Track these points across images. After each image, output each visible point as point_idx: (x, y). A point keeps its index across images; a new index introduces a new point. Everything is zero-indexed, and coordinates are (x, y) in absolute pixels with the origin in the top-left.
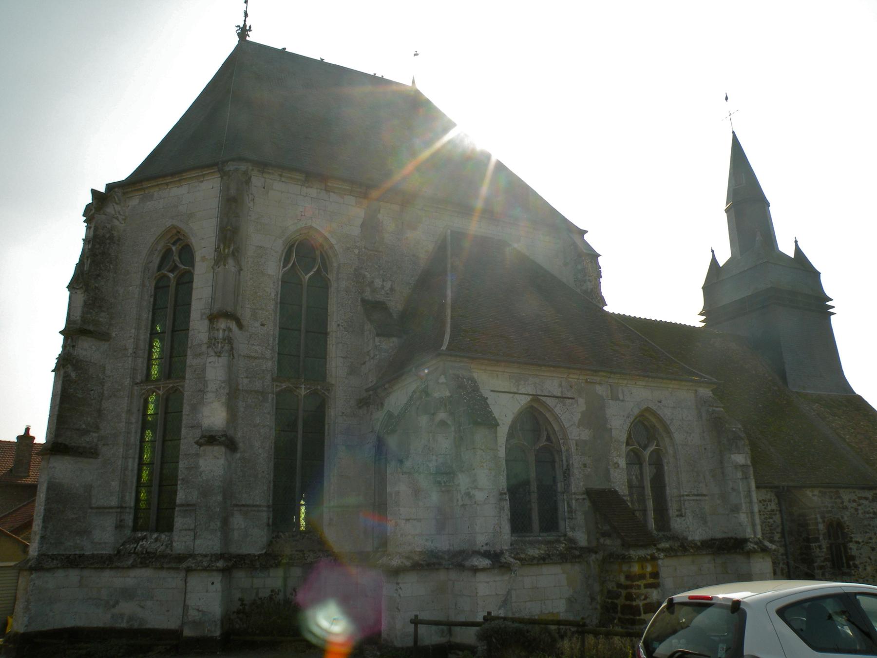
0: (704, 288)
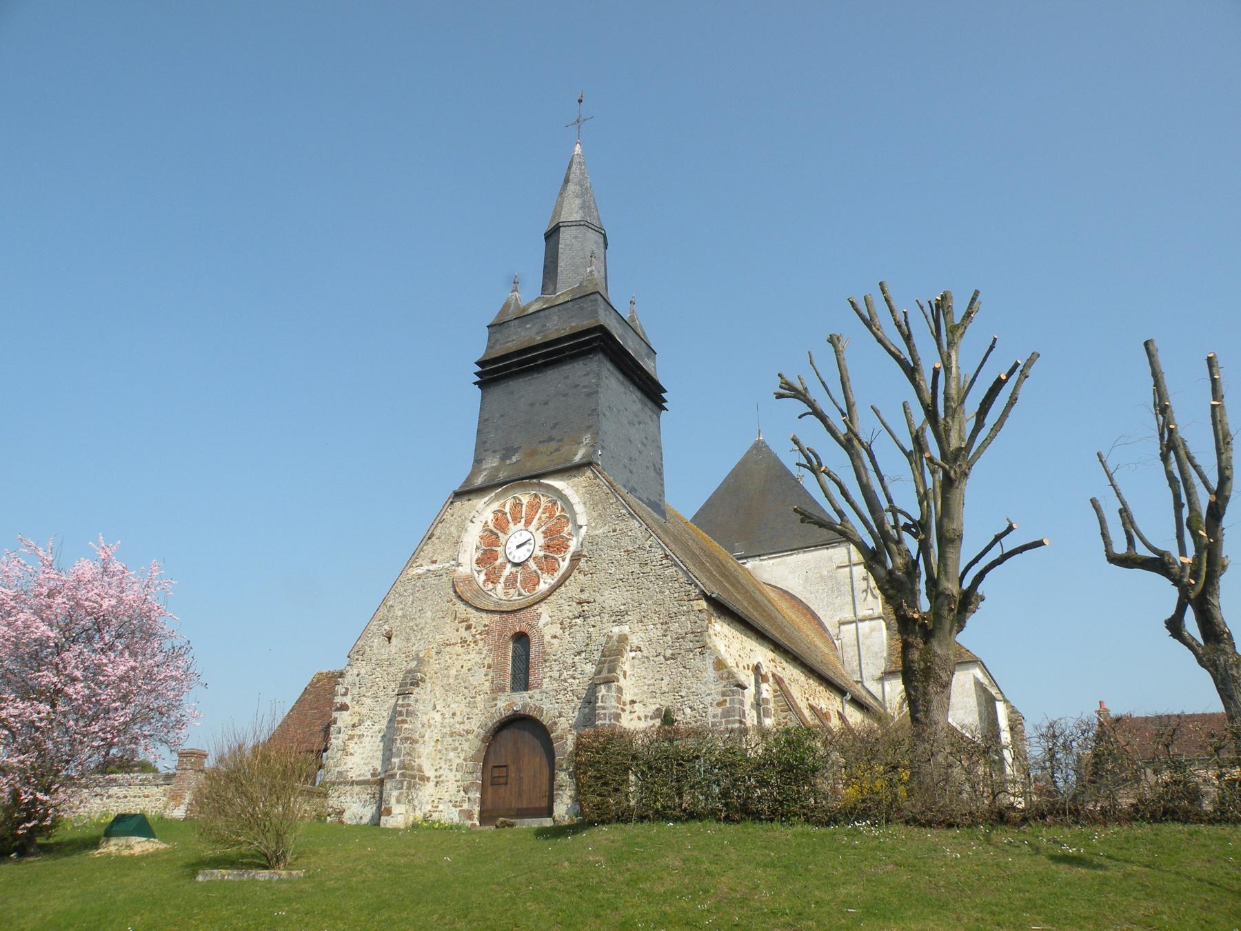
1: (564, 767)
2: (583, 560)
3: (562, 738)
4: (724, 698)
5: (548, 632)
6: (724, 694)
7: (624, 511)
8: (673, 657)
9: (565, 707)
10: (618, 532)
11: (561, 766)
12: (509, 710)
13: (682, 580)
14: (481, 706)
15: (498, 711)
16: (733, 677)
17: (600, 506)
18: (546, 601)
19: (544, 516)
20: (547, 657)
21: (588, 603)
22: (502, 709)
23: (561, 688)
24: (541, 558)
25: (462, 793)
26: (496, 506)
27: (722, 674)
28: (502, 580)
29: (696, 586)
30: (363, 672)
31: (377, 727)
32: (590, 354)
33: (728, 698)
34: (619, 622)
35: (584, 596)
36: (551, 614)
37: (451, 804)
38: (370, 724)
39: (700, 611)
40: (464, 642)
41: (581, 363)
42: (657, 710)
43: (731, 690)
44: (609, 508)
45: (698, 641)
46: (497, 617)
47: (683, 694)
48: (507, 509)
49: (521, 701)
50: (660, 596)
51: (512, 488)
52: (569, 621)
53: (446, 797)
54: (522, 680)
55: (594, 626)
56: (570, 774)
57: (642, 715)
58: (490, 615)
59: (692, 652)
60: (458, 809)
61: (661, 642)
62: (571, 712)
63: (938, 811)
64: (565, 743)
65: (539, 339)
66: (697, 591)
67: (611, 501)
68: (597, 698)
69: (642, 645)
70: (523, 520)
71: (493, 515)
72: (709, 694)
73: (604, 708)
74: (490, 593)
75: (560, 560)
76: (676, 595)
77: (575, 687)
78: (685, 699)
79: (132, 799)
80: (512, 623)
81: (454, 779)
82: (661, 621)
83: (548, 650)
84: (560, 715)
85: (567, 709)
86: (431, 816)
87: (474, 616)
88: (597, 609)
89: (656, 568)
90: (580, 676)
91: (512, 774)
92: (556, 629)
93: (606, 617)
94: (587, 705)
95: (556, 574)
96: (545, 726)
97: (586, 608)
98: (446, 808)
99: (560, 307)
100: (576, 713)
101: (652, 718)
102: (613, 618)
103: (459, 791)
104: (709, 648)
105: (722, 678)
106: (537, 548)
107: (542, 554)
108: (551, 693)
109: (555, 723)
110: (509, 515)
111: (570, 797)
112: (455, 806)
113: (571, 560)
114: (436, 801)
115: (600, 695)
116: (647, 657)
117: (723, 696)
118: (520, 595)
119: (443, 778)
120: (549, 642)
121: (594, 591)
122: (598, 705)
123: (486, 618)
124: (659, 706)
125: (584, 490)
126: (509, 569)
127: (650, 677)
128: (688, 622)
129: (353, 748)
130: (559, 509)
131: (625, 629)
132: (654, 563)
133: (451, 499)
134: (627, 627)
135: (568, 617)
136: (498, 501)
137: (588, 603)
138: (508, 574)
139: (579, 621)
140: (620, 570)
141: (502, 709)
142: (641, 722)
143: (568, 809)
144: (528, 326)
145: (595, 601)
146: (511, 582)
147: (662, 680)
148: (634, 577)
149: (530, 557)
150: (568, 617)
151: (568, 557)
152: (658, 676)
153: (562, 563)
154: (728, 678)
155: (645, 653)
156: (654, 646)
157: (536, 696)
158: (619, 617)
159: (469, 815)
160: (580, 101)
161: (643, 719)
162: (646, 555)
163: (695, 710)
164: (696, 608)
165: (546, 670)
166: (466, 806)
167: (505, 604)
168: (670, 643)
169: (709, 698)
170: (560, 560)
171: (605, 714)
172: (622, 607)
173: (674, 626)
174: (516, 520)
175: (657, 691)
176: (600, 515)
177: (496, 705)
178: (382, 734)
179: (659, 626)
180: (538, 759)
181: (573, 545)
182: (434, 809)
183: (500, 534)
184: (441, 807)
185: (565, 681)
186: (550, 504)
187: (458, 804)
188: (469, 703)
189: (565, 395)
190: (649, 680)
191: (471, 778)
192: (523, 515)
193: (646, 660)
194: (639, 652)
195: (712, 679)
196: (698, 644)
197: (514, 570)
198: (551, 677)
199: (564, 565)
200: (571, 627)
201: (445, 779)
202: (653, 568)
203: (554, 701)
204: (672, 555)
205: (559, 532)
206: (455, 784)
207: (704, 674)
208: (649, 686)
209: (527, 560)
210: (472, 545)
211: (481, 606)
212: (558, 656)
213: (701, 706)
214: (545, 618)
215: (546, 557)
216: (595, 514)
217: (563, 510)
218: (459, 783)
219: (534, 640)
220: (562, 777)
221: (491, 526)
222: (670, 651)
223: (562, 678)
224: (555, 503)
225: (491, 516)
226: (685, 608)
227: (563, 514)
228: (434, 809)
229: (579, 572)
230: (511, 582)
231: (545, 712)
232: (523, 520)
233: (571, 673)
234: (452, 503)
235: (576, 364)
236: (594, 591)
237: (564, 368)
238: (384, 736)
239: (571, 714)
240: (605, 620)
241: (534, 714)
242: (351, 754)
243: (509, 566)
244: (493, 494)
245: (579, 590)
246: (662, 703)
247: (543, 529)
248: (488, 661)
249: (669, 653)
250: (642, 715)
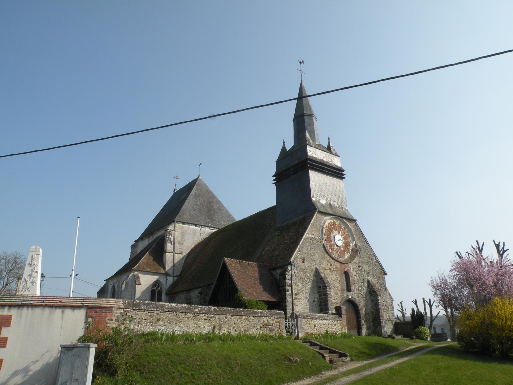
0: (277, 162)
14: (339, 294)
30: (296, 272)
31: (305, 296)
35: (360, 264)
38: (302, 294)
40: (330, 270)
54: (349, 289)
63: (184, 324)
79: (331, 326)
87: (332, 262)
129: (297, 303)
136: (330, 220)
139: (360, 272)
158: (369, 274)
178: (307, 299)
188: (336, 293)
209: (341, 246)
210: (450, 266)
238: (308, 300)
242: (297, 306)
244: (332, 217)
248: (339, 279)
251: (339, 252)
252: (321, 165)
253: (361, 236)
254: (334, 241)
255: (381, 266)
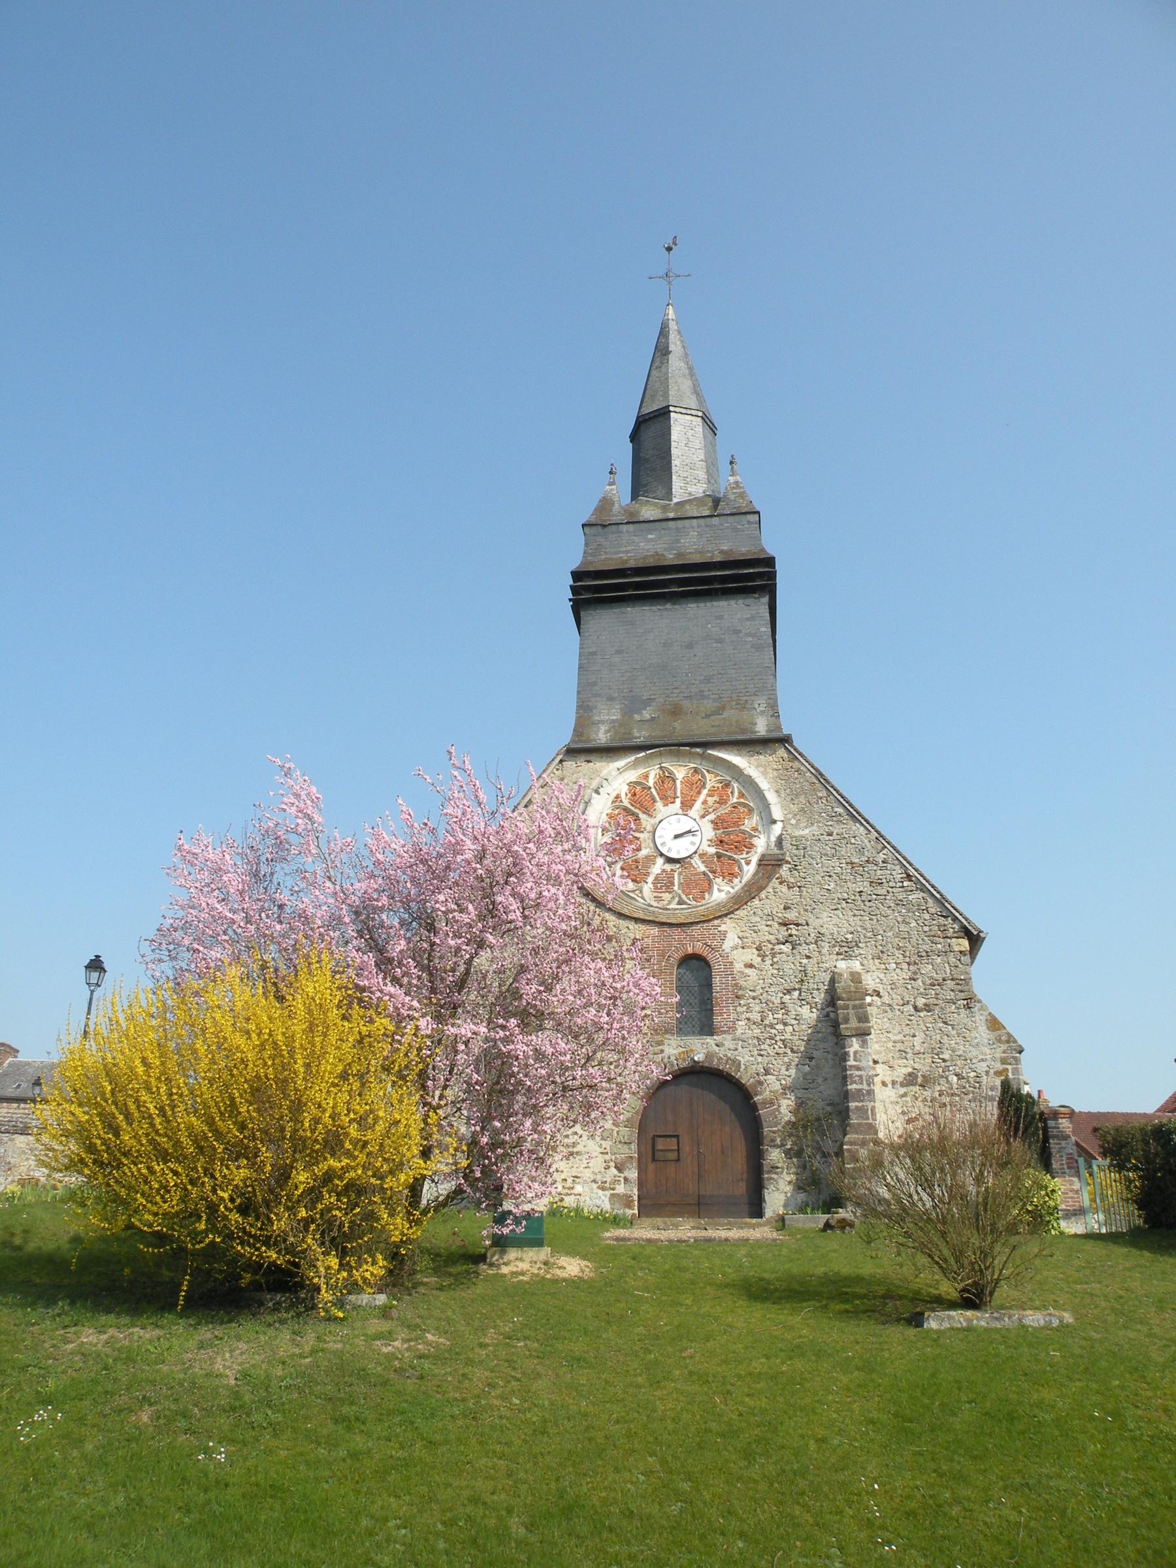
1: (778, 1141)
2: (785, 867)
3: (772, 1103)
4: (1005, 1066)
5: (740, 958)
6: (1004, 1061)
7: (840, 810)
8: (928, 1008)
9: (774, 1062)
10: (835, 836)
11: (773, 1140)
12: (684, 1060)
13: (932, 910)
15: (666, 1060)
16: (1015, 1041)
17: (802, 799)
18: (732, 916)
19: (711, 800)
20: (740, 993)
21: (797, 925)
22: (673, 1058)
23: (766, 1035)
24: (712, 856)
25: (614, 1171)
26: (633, 775)
27: (1000, 1036)
28: (650, 879)
29: (955, 919)
32: (755, 593)
33: (1009, 1067)
34: (847, 956)
35: (791, 915)
36: (741, 934)
37: (595, 1186)
39: (961, 952)
41: (740, 602)
42: (910, 1074)
43: (1013, 1057)
44: (817, 803)
45: (962, 991)
46: (655, 931)
47: (946, 1056)
48: (651, 783)
49: (700, 1049)
50: (903, 927)
51: (660, 754)
52: (770, 946)
53: (587, 1175)
55: (808, 957)
56: (788, 1153)
57: (888, 1080)
58: (642, 927)
59: (954, 1003)
60: (608, 1193)
61: (909, 987)
62: (784, 1068)
64: (778, 1110)
65: (670, 558)
66: (956, 926)
67: (820, 794)
68: (847, 1054)
69: (880, 988)
70: (678, 801)
71: (627, 787)
72: (982, 1060)
73: (858, 1068)
74: (632, 895)
75: (743, 862)
76: (926, 929)
77: (788, 1036)
78: (948, 1064)
80: (680, 940)
81: (599, 1150)
82: (907, 960)
83: (742, 983)
84: (767, 1072)
85: (778, 1064)
86: (562, 1200)
88: (812, 935)
89: (894, 890)
90: (794, 1022)
91: (686, 1148)
92: (752, 955)
93: (826, 948)
94: (807, 1061)
95: (736, 881)
96: (743, 1085)
97: (794, 932)
98: (586, 1189)
99: (702, 521)
100: (793, 1072)
101: (902, 1085)
102: (837, 949)
103: (607, 1168)
104: (979, 1001)
105: (1000, 1041)
106: (705, 843)
107: (712, 850)
108: (750, 1041)
109: (760, 1083)
110: (653, 790)
111: (790, 1182)
112: (603, 1189)
113: (759, 865)
114: (570, 1180)
115: (851, 1051)
116: (890, 1005)
117: (1002, 1064)
118: (681, 902)
119: (578, 1148)
120: (742, 973)
121: (806, 910)
122: (849, 1063)
123: (637, 930)
124: (910, 1070)
125: (775, 773)
126: (659, 866)
127: (896, 1032)
128: (946, 965)
130: (736, 794)
131: (856, 965)
132: (891, 884)
133: (560, 757)
134: (858, 963)
135: (769, 941)
137: (797, 925)
138: (659, 871)
139: (786, 948)
140: (842, 887)
141: (673, 1058)
142: (887, 1089)
143: (788, 1199)
144: (650, 536)
145: (807, 924)
146: (664, 884)
147: (914, 1036)
148: (863, 898)
149: (695, 853)
150: (769, 941)
151: (755, 860)
152: (907, 1030)
153: (745, 867)
154: (1008, 1042)
155: (886, 999)
156: (899, 991)
157: (726, 1043)
158: (846, 949)
159: (627, 1201)
160: (669, 249)
161: (890, 1086)
162: (879, 872)
163: (963, 1078)
164: (956, 948)
165: (739, 1009)
166: (621, 1189)
167: (660, 914)
168: (922, 990)
169: (984, 1064)
170: (743, 862)
171: (861, 1077)
172: (849, 936)
173: (927, 969)
174: (668, 800)
175: (908, 1050)
176: (803, 810)
177: (662, 1051)
179: (905, 966)
180: (727, 1129)
181: (761, 844)
182: (567, 1191)
183: (641, 816)
184: (578, 1189)
185: (772, 1026)
186: (720, 785)
187: (607, 1185)
189: (719, 641)
190: (896, 1035)
191: (627, 1151)
192: (679, 794)
193: (888, 1008)
194: (875, 998)
195: (986, 1041)
196: (962, 995)
197: (668, 867)
198: (748, 1019)
199: (750, 870)
200: (774, 955)
201: (583, 1149)
202: (890, 889)
203: (756, 1052)
204: (918, 876)
205: (736, 824)
206: (601, 1158)
207: (974, 1034)
208: (895, 1042)
209: (690, 857)
211: (625, 911)
212: (758, 993)
213: (972, 1074)
214: (731, 940)
215: (719, 856)
216: (794, 808)
217: (741, 795)
218: (607, 1157)
219: (717, 968)
220: (775, 1156)
221: (626, 803)
222: (924, 1001)
223: (767, 1022)
224: (727, 785)
225: (625, 789)
226: (939, 946)
227: (742, 800)
228: (567, 1191)
229: (781, 883)
230: (664, 884)
231: (743, 1067)
232: (678, 801)
233: (780, 1016)
234: (561, 761)
235: (732, 602)
236: (806, 910)
237: (715, 604)
239: (783, 1071)
240: (825, 951)
241: (727, 1068)
243: (660, 861)
244: (633, 758)
245: (782, 907)
246: (916, 1066)
247: (712, 817)
249: (921, 1002)
250: (888, 1080)
251: (680, 884)
252: (719, 570)
253: (823, 793)
254: (652, 845)
255: (941, 901)
